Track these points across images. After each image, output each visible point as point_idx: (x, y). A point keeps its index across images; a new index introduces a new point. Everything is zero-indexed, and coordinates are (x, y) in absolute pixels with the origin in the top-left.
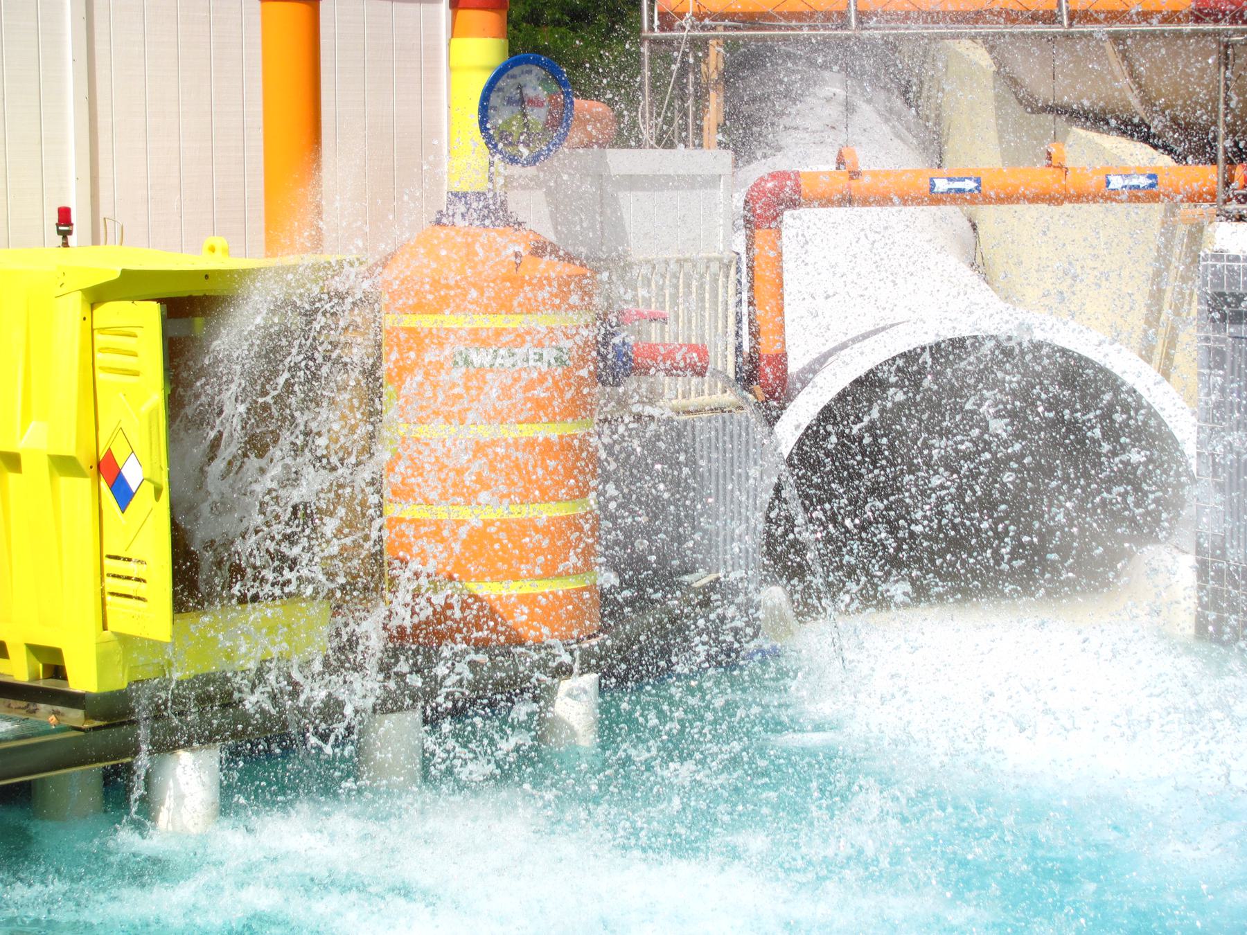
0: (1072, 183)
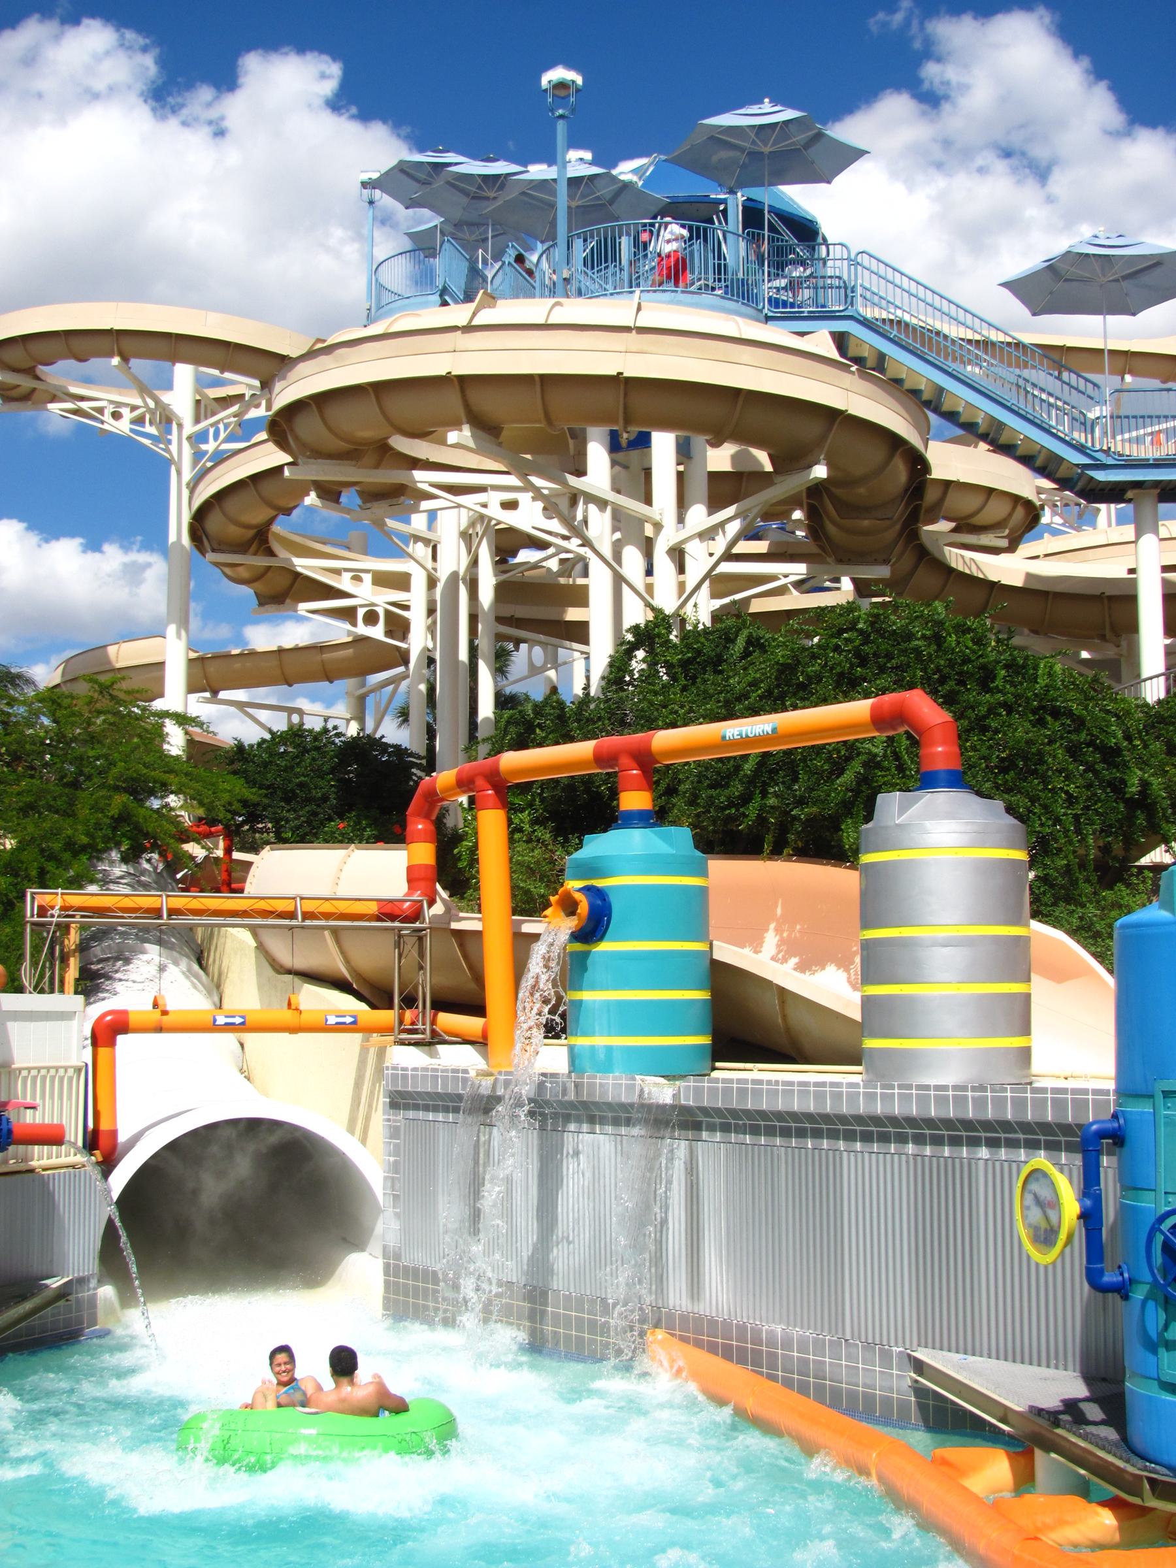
0: (305, 1019)
